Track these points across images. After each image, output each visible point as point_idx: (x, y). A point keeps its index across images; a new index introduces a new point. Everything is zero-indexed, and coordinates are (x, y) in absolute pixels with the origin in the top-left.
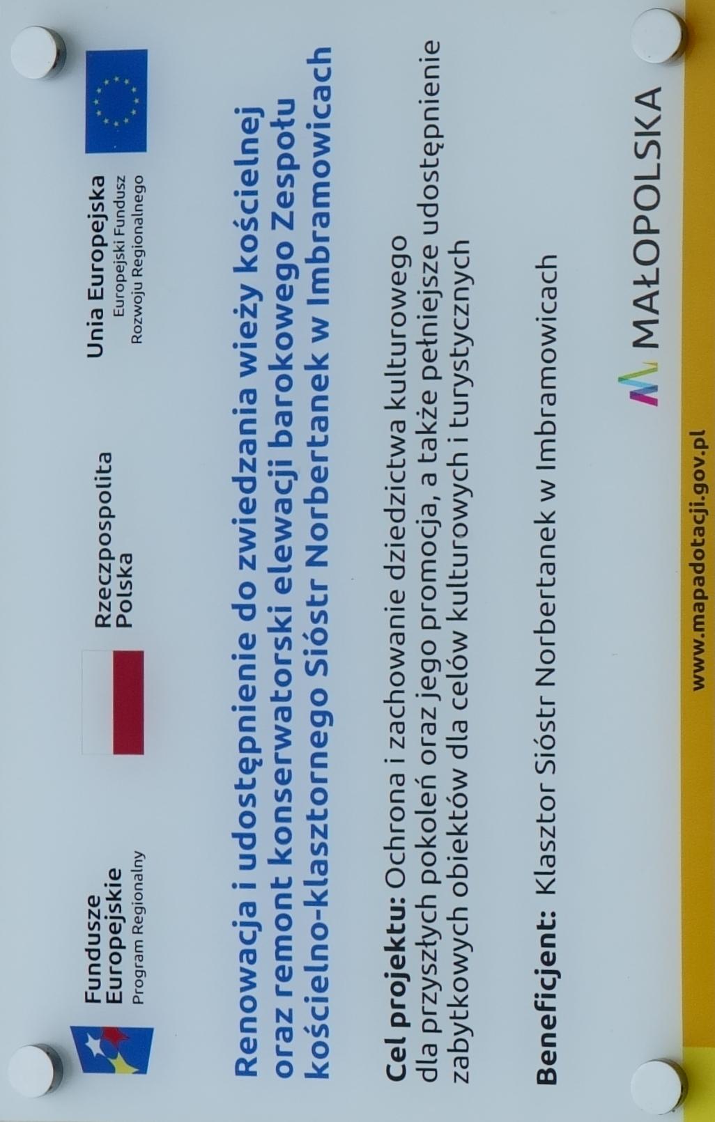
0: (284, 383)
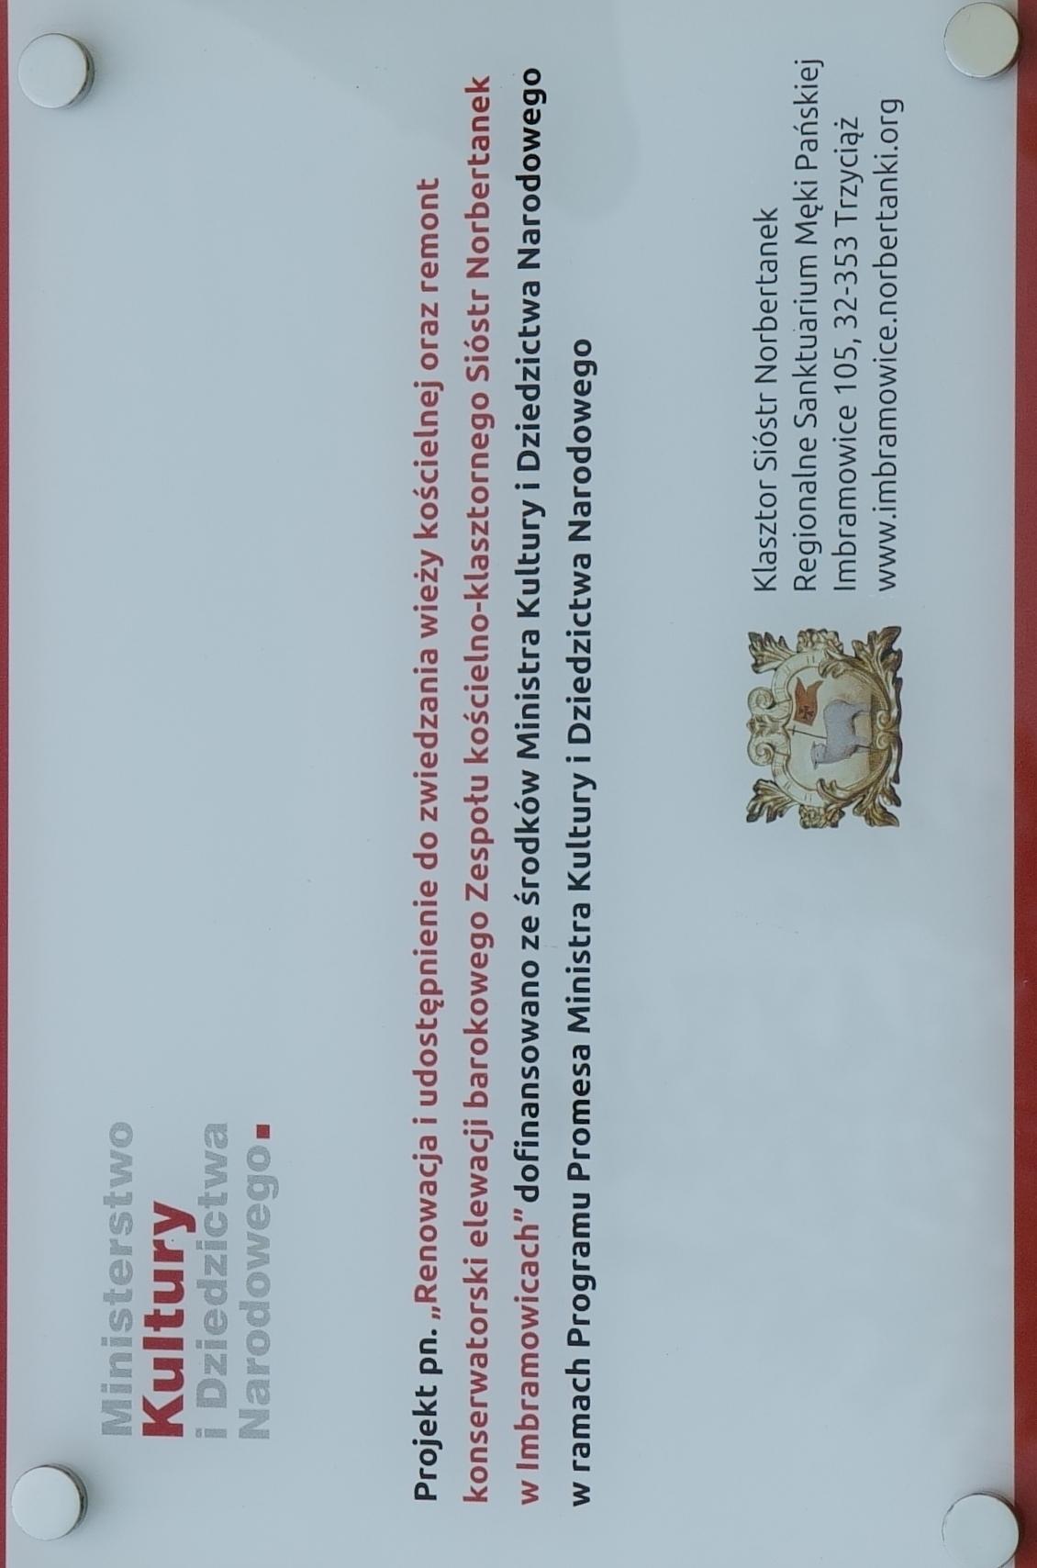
0: (479, 1047)
